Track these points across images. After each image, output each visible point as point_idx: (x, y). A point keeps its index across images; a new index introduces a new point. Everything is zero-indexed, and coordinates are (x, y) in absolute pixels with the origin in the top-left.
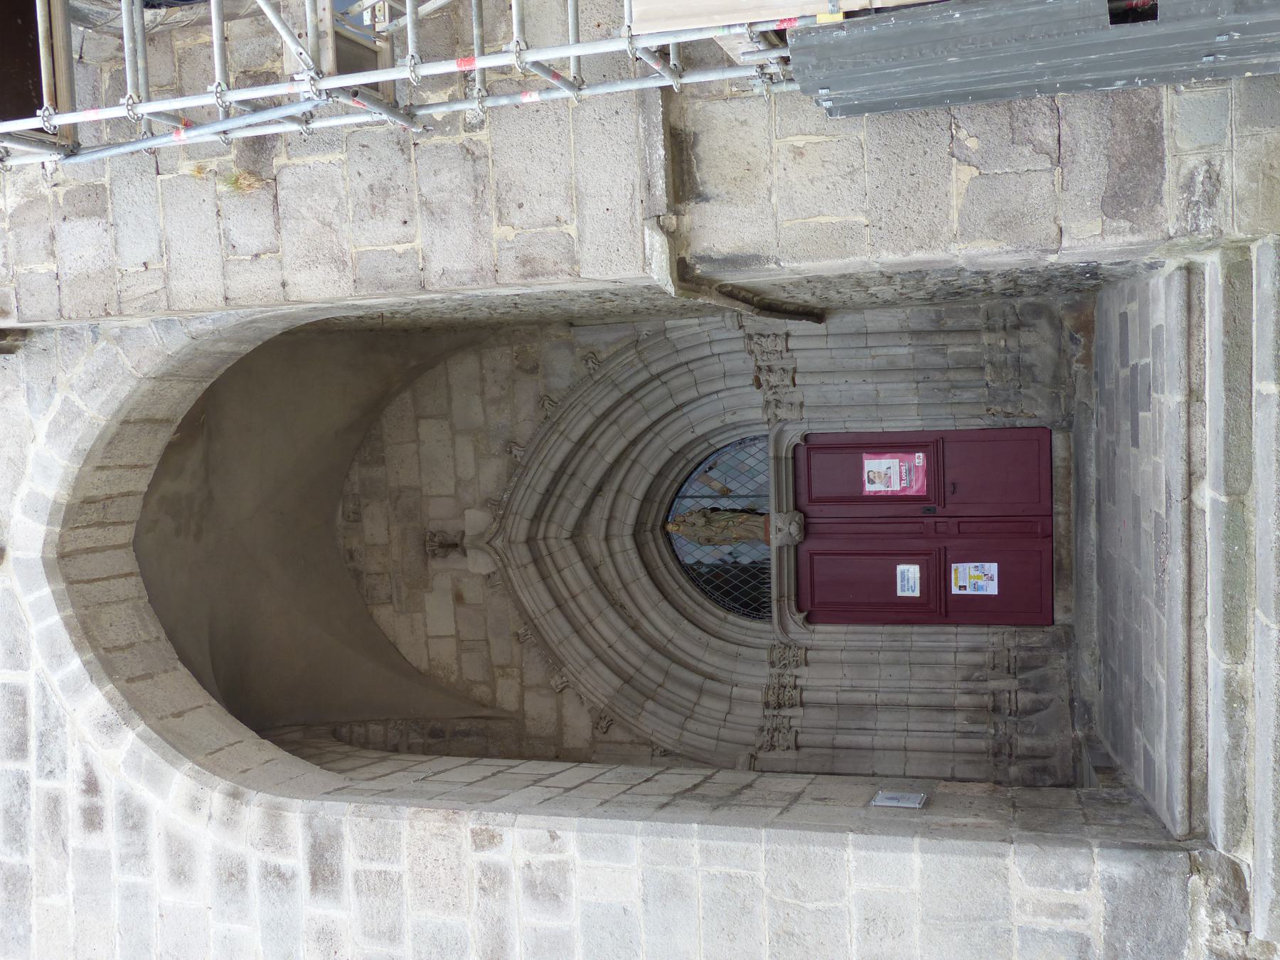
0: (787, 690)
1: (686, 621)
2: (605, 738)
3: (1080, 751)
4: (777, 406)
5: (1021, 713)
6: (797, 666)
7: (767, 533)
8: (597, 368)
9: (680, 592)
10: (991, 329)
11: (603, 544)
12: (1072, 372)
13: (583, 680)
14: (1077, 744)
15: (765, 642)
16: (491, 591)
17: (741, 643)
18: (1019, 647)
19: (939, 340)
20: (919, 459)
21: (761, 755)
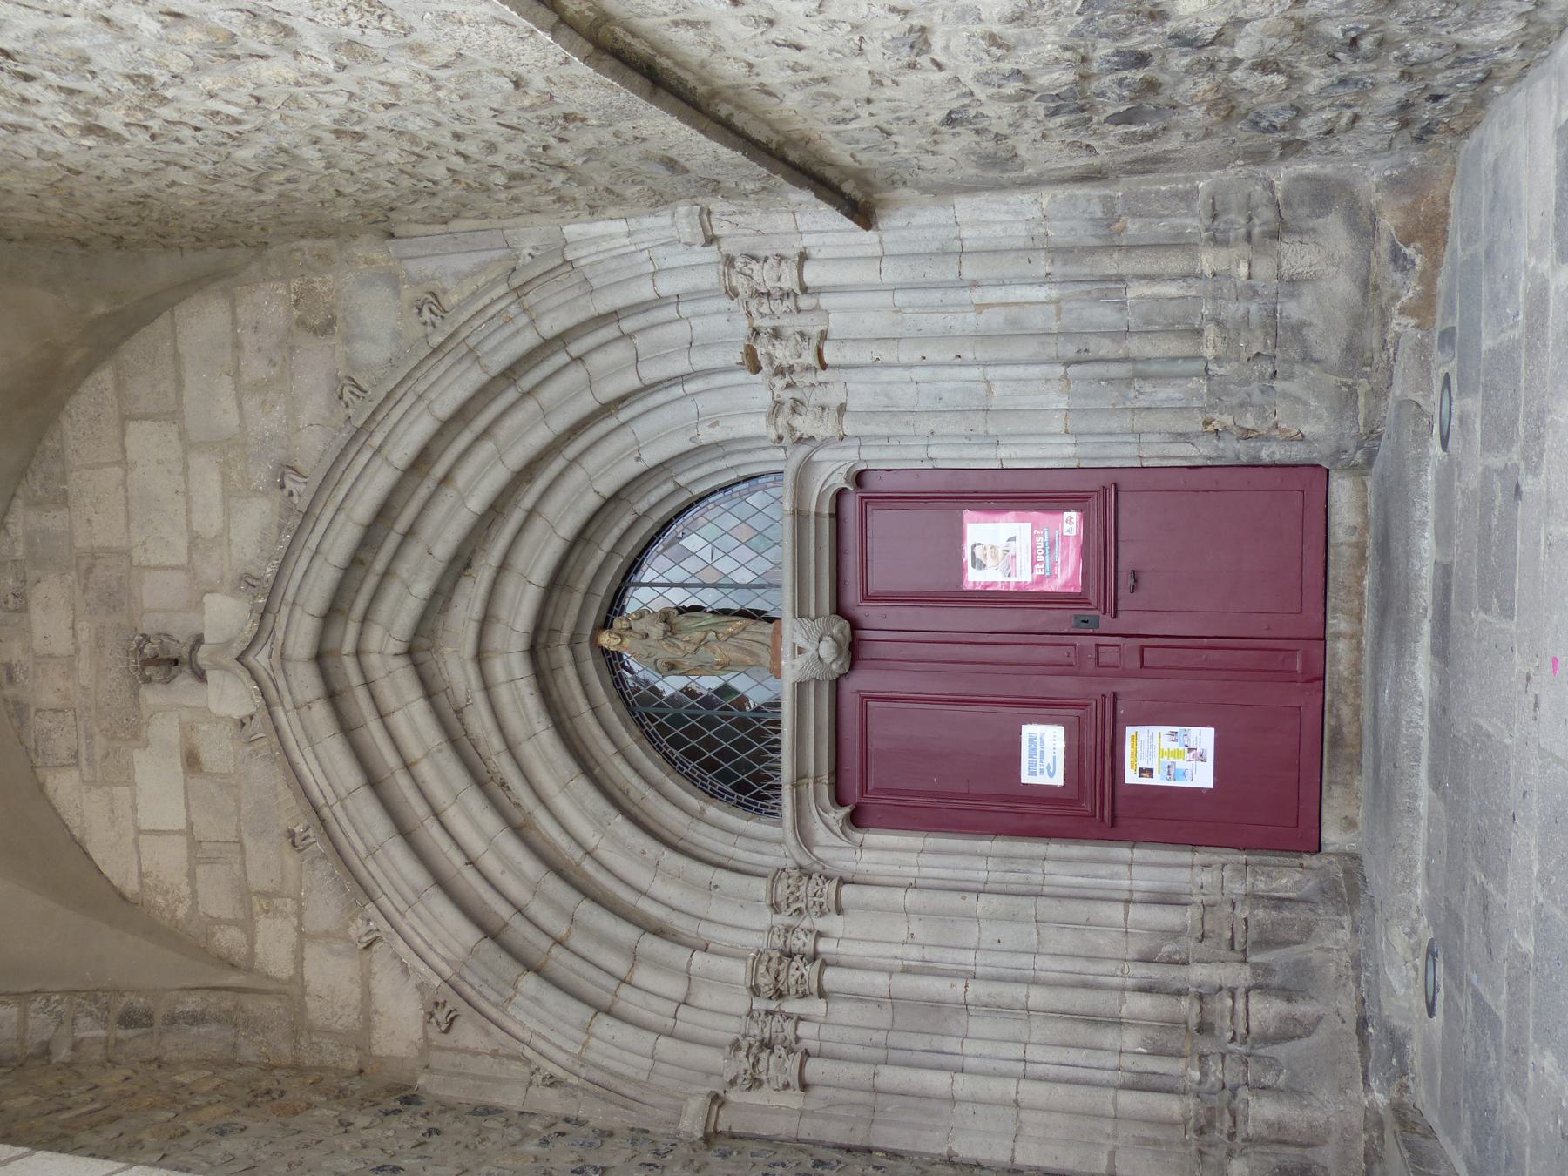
0: (794, 965)
1: (620, 818)
2: (446, 1040)
3: (1381, 1138)
4: (794, 411)
5: (1255, 1040)
6: (822, 914)
7: (776, 656)
8: (438, 321)
9: (618, 761)
10: (1218, 240)
11: (471, 669)
12: (1389, 337)
13: (407, 929)
14: (1374, 1121)
15: (770, 860)
16: (248, 749)
17: (724, 861)
18: (1255, 898)
19: (1110, 265)
20: (1070, 523)
21: (734, 1096)
